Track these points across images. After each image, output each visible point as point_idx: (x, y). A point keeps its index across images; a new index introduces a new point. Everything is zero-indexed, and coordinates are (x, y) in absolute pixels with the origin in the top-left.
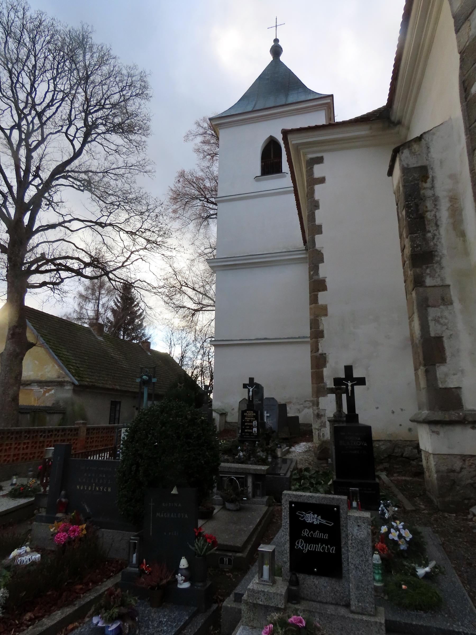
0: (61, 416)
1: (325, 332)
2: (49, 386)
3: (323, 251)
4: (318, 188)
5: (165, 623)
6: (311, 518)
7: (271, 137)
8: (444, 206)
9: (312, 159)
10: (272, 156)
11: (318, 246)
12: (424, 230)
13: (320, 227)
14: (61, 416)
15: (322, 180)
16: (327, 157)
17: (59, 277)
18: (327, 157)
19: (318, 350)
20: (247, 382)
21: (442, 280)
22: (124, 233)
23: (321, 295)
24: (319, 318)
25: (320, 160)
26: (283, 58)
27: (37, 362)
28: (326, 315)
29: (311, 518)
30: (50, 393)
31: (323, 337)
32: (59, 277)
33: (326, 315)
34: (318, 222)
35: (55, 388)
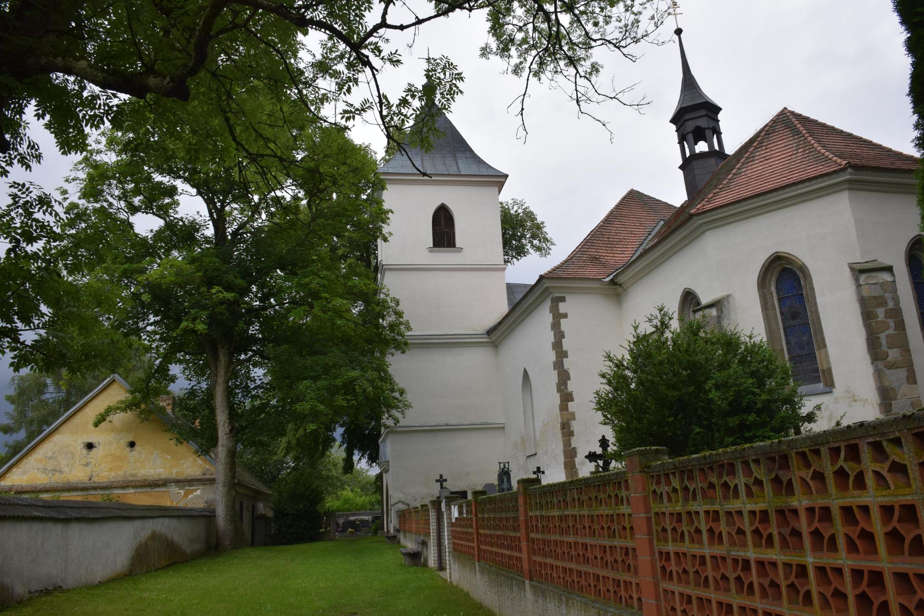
1: (575, 432)
2: (193, 486)
3: (570, 371)
4: (562, 321)
7: (443, 204)
9: (557, 297)
15: (565, 316)
16: (568, 297)
18: (568, 297)
22: (398, 303)
23: (570, 404)
24: (570, 422)
25: (563, 299)
27: (169, 457)
28: (575, 419)
30: (195, 494)
31: (573, 435)
33: (575, 419)
34: (564, 348)
35: (201, 487)
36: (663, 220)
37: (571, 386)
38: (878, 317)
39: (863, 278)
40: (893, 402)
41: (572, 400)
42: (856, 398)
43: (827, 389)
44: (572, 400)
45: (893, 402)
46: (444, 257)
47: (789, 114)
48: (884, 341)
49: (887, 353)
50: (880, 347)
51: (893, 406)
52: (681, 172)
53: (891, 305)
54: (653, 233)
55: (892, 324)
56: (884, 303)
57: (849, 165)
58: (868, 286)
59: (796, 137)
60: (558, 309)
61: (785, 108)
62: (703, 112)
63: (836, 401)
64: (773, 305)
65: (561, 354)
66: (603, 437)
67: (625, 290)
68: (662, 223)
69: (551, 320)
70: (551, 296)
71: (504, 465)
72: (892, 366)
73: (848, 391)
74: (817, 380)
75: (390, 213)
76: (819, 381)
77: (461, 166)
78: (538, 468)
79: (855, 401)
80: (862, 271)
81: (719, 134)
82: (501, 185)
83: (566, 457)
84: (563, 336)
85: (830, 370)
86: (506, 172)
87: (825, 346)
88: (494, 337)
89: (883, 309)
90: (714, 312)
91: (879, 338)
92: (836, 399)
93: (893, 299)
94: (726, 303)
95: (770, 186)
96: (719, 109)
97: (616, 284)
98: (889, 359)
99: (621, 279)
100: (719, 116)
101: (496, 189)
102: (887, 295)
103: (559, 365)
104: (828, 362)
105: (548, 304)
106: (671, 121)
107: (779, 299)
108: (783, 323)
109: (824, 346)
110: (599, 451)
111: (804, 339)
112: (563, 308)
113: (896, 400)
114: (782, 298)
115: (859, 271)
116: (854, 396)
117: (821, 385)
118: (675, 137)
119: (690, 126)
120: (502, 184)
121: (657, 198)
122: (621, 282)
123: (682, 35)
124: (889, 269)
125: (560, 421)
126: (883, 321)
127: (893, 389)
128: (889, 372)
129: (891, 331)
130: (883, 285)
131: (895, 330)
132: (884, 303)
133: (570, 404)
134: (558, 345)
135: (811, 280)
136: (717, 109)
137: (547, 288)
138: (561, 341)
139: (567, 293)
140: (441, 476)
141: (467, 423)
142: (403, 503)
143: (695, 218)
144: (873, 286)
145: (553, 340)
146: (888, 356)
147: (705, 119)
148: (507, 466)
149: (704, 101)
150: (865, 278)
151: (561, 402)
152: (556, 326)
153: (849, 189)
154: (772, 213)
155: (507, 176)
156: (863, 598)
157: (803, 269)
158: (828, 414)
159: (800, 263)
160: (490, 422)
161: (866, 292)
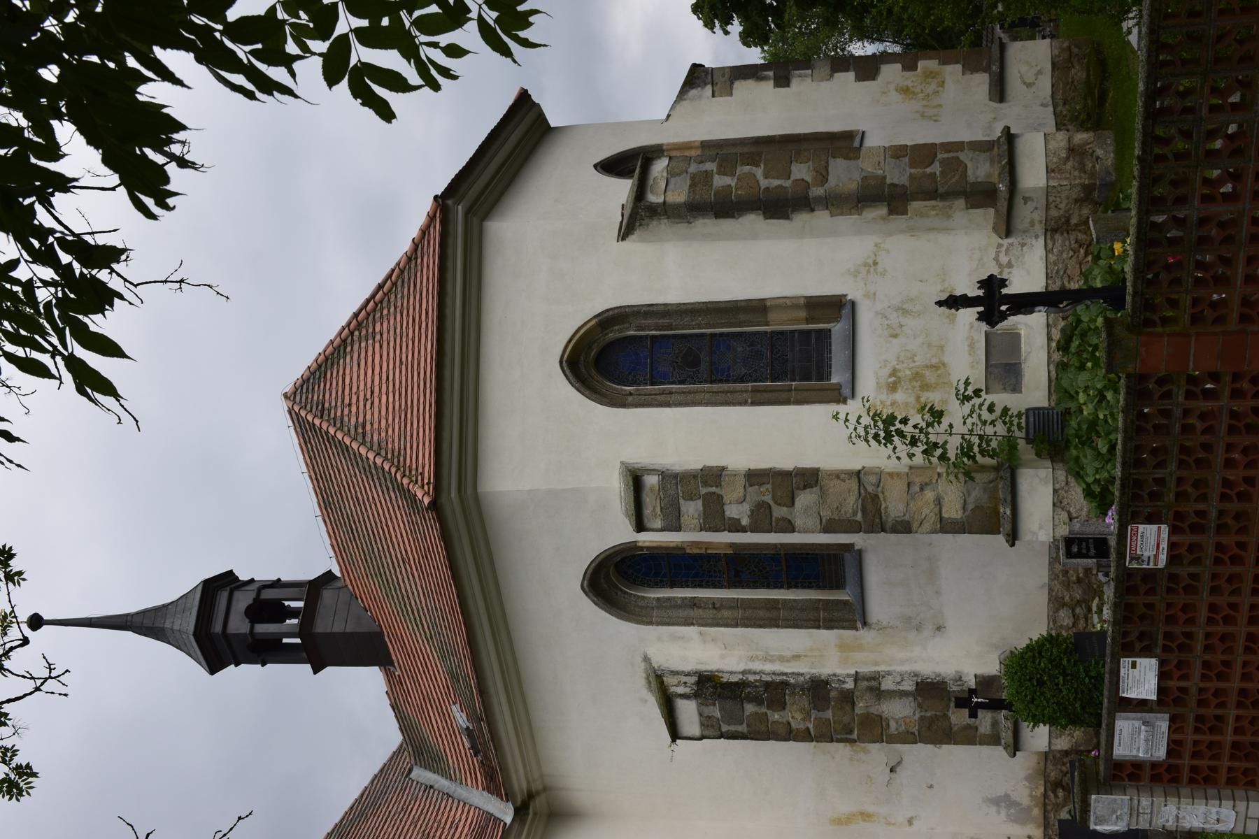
6: (1075, 549)
8: (757, 666)
12: (785, 684)
21: (848, 676)
29: (1075, 549)
39: (654, 198)
40: (888, 181)
42: (870, 261)
43: (846, 311)
45: (888, 181)
48: (776, 182)
50: (785, 188)
51: (896, 181)
56: (708, 175)
58: (669, 193)
59: (349, 349)
62: (224, 595)
63: (872, 296)
64: (662, 393)
67: (545, 789)
73: (856, 273)
75: (8, 796)
79: (875, 263)
89: (716, 177)
91: (768, 188)
92: (866, 295)
96: (231, 571)
98: (809, 179)
99: (519, 783)
100: (241, 579)
102: (693, 168)
106: (213, 670)
111: (740, 349)
113: (885, 177)
114: (652, 377)
116: (866, 265)
117: (838, 329)
119: (239, 625)
121: (356, 795)
123: (45, 618)
126: (738, 179)
127: (864, 179)
131: (757, 165)
132: (708, 175)
136: (230, 573)
143: (444, 500)
144: (671, 186)
147: (237, 594)
149: (200, 587)
154: (482, 360)
156: (1250, 429)
157: (609, 320)
158: (895, 315)
159: (593, 322)
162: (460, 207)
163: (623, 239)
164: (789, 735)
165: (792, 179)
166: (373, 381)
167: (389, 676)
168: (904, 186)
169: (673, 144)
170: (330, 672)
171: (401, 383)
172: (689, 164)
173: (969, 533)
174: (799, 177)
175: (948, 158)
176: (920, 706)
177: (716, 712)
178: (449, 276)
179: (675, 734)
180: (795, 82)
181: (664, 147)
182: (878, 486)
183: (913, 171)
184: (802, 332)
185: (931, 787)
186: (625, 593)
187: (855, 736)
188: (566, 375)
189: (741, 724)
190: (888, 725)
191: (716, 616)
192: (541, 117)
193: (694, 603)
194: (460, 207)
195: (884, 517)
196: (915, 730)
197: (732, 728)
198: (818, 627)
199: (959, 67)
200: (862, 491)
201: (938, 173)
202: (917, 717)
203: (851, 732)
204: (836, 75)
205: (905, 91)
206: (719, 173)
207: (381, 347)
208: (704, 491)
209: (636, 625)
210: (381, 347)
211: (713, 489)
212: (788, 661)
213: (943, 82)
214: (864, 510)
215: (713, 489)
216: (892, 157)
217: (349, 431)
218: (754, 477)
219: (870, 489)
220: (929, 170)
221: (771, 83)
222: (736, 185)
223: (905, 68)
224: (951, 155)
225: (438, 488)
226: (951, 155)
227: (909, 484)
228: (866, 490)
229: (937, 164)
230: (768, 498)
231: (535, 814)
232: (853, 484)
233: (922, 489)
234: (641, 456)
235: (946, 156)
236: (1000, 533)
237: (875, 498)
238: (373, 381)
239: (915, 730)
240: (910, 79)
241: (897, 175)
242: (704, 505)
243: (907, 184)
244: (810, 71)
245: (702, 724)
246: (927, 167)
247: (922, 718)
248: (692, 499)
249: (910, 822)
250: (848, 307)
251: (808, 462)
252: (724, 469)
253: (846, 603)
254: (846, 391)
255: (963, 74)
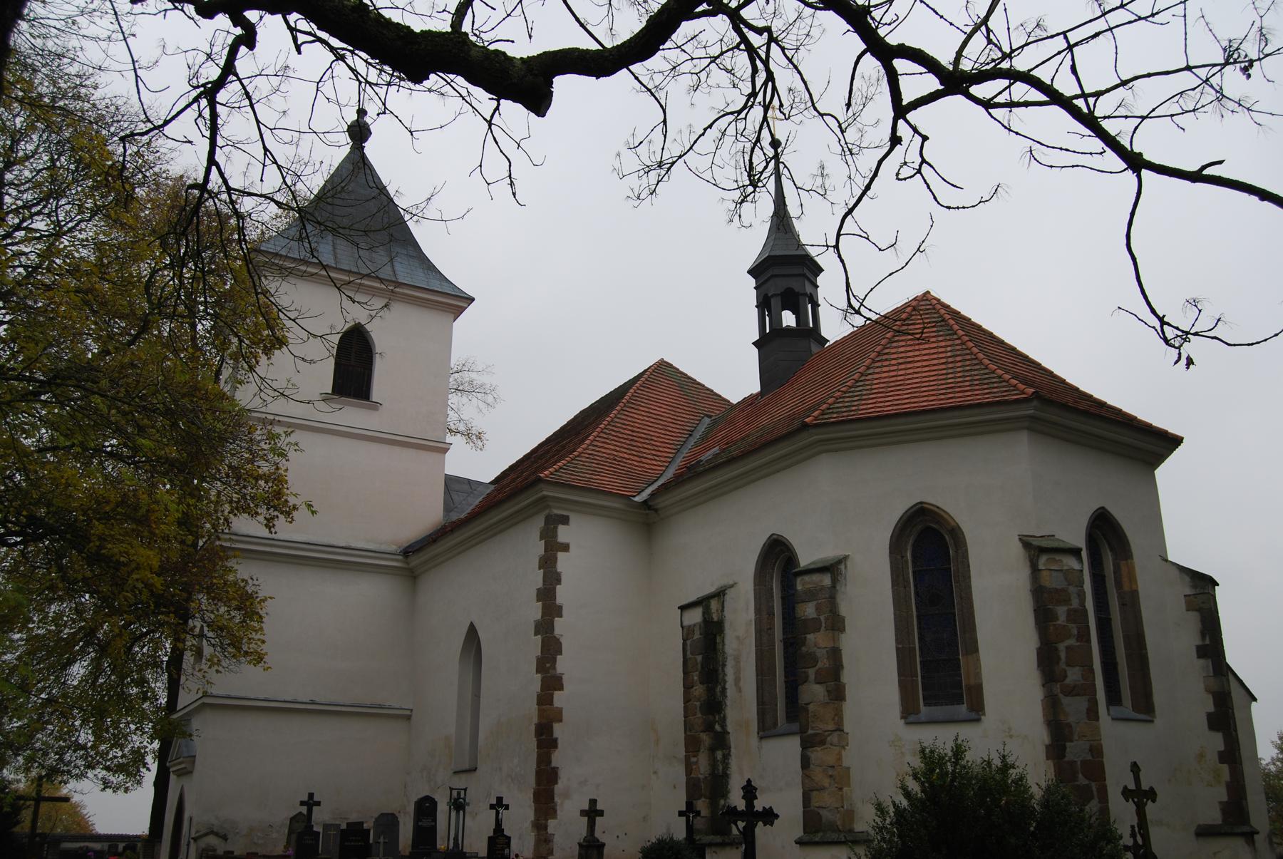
0: (900, 177)
1: (559, 742)
3: (563, 641)
4: (561, 555)
5: (147, 263)
10: (372, 832)
11: (557, 631)
13: (560, 608)
14: (900, 177)
15: (566, 548)
16: (574, 518)
17: (834, 247)
18: (574, 518)
19: (550, 762)
20: (494, 802)
23: (557, 694)
25: (565, 520)
26: (370, 148)
32: (834, 247)
34: (559, 601)
36: (710, 417)
37: (563, 665)
38: (1057, 619)
39: (1043, 562)
40: (1068, 744)
41: (561, 688)
43: (973, 715)
44: (561, 688)
45: (1068, 744)
46: (350, 415)
47: (935, 302)
48: (1063, 655)
49: (1066, 671)
51: (1068, 750)
52: (755, 351)
53: (1075, 603)
54: (697, 435)
55: (1075, 632)
56: (1067, 601)
57: (1036, 396)
60: (555, 536)
61: (928, 292)
65: (551, 609)
66: (749, 781)
68: (707, 420)
69: (541, 551)
70: (547, 512)
71: (459, 794)
72: (1071, 691)
74: (958, 700)
76: (960, 702)
77: (398, 267)
78: (500, 799)
80: (1043, 550)
81: (816, 305)
82: (458, 311)
83: (538, 782)
84: (559, 581)
85: (979, 688)
86: (470, 293)
87: (976, 650)
88: (415, 561)
89: (1065, 608)
90: (826, 580)
93: (1079, 595)
94: (842, 567)
95: (925, 404)
96: (821, 270)
97: (650, 508)
98: (1068, 681)
99: (662, 502)
101: (452, 316)
102: (1072, 589)
103: (545, 627)
104: (978, 675)
105: (539, 522)
106: (750, 272)
107: (914, 572)
108: (917, 608)
109: (973, 649)
110: (759, 805)
112: (563, 534)
113: (1072, 741)
115: (1036, 550)
116: (1010, 729)
117: (963, 709)
118: (751, 297)
120: (462, 310)
122: (659, 506)
124: (1076, 552)
125: (535, 720)
126: (1064, 626)
127: (1069, 726)
128: (1065, 700)
129: (1072, 642)
130: (1067, 573)
132: (1067, 601)
133: (557, 694)
134: (547, 596)
135: (967, 551)
137: (544, 497)
138: (555, 589)
139: (572, 511)
140: (311, 795)
141: (348, 703)
142: (217, 834)
144: (1054, 574)
145: (540, 585)
146: (1066, 676)
148: (462, 796)
150: (1047, 560)
151: (542, 690)
152: (548, 563)
153: (1030, 429)
155: (473, 300)
159: (953, 523)
160: (387, 704)
161: (1049, 581)
162: (1032, 411)
163: (1020, 539)
164: (688, 687)
165: (1067, 668)
166: (918, 361)
167: (758, 395)
168: (1065, 756)
169: (1133, 567)
170: (755, 351)
171: (909, 384)
172: (1077, 586)
173: (804, 812)
174: (1069, 673)
175: (1092, 791)
176: (706, 777)
177: (697, 636)
178: (976, 411)
179: (683, 608)
180: (1202, 661)
181: (1129, 561)
182: (831, 744)
183: (1079, 763)
184: (960, 682)
185: (675, 787)
186: (774, 565)
187: (688, 733)
188: (912, 507)
189: (692, 654)
190: (694, 756)
191: (763, 630)
192: (1160, 458)
193: (771, 614)
194: (1032, 411)
195: (810, 749)
196: (692, 776)
197: (688, 647)
198: (758, 705)
199: (1225, 798)
200: (827, 733)
201: (1076, 783)
202: (700, 776)
203: (690, 731)
204: (1211, 696)
205: (1201, 756)
206: (1069, 611)
207: (943, 364)
208: (822, 618)
209: (1085, 526)
210: (943, 364)
211: (823, 625)
212: (736, 685)
213: (1211, 786)
214: (816, 735)
215: (823, 625)
216: (1091, 746)
217: (887, 348)
218: (835, 654)
219: (829, 739)
220: (1080, 775)
221: (1199, 642)
222: (1060, 625)
223: (1220, 753)
224: (1095, 793)
225: (817, 426)
226: (1095, 793)
227: (833, 767)
228: (829, 735)
229: (1086, 782)
230: (820, 665)
231: (647, 514)
232: (831, 727)
233: (831, 776)
234: (853, 571)
235: (1094, 789)
236: (805, 833)
237: (822, 742)
238: (918, 361)
239: (692, 776)
240: (1212, 758)
241: (1076, 750)
242: (813, 619)
243: (1066, 759)
244: (1212, 674)
245: (690, 626)
246: (1082, 774)
247: (699, 779)
248: (817, 609)
249: (655, 773)
250: (976, 717)
251: (849, 693)
252: (843, 630)
253: (775, 724)
254: (911, 719)
255: (1220, 803)
